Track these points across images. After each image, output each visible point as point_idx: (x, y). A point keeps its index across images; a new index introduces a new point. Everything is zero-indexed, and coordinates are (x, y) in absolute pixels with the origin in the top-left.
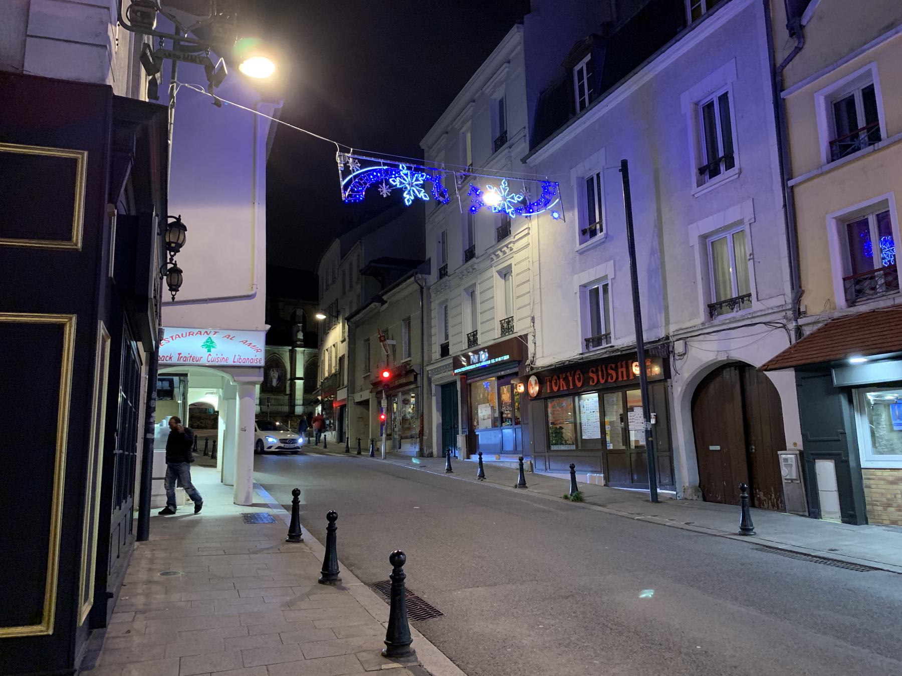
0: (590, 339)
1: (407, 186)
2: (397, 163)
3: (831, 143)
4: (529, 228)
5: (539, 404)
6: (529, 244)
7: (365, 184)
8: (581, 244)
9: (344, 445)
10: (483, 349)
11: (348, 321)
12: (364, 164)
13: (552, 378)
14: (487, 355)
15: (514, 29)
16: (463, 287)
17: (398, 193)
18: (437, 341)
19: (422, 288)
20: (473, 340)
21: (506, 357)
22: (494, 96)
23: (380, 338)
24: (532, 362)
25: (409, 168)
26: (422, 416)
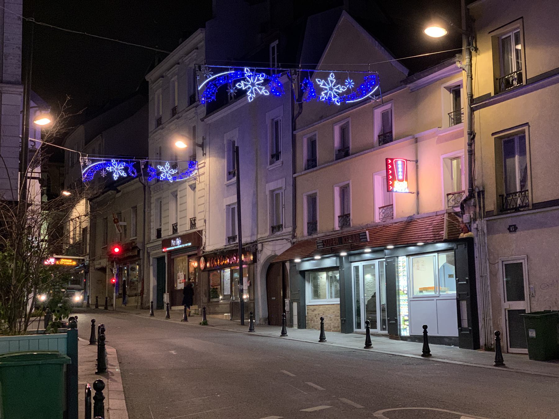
0: (231, 237)
2: (110, 159)
3: (308, 161)
4: (205, 163)
5: (206, 274)
6: (205, 173)
7: (94, 171)
10: (178, 237)
11: (90, 202)
12: (93, 161)
13: (211, 259)
14: (180, 241)
15: (199, 31)
16: (170, 191)
18: (154, 227)
19: (145, 187)
20: (175, 230)
21: (190, 244)
22: (190, 66)
23: (114, 220)
24: (204, 248)
26: (143, 280)
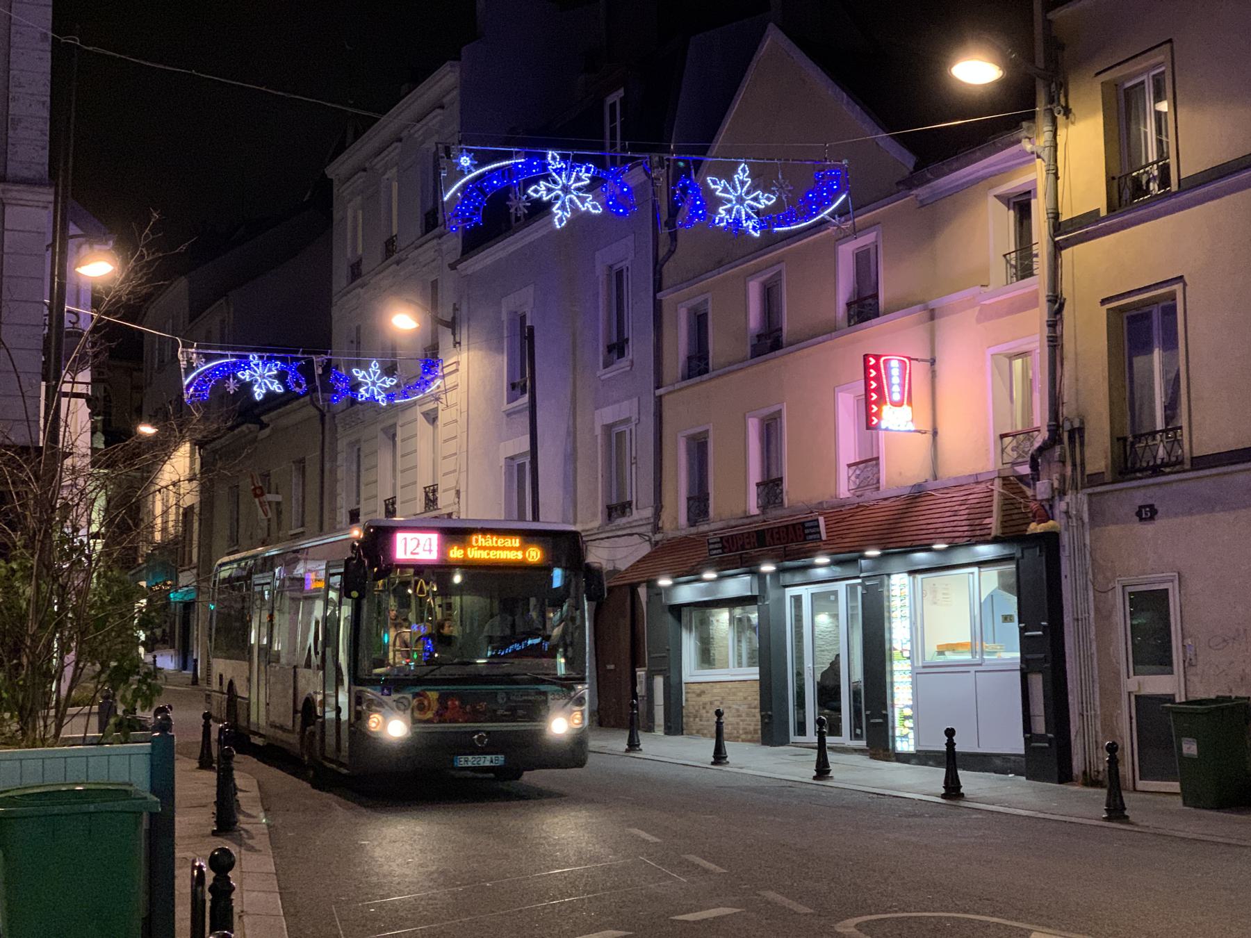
1: (258, 378)
2: (247, 353)
3: (689, 358)
4: (457, 363)
6: (457, 385)
7: (210, 381)
8: (508, 403)
9: (188, 673)
12: (209, 358)
15: (446, 67)
17: (246, 387)
19: (323, 416)
25: (261, 358)
